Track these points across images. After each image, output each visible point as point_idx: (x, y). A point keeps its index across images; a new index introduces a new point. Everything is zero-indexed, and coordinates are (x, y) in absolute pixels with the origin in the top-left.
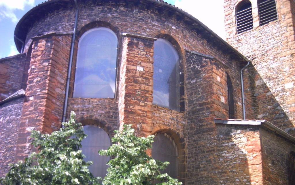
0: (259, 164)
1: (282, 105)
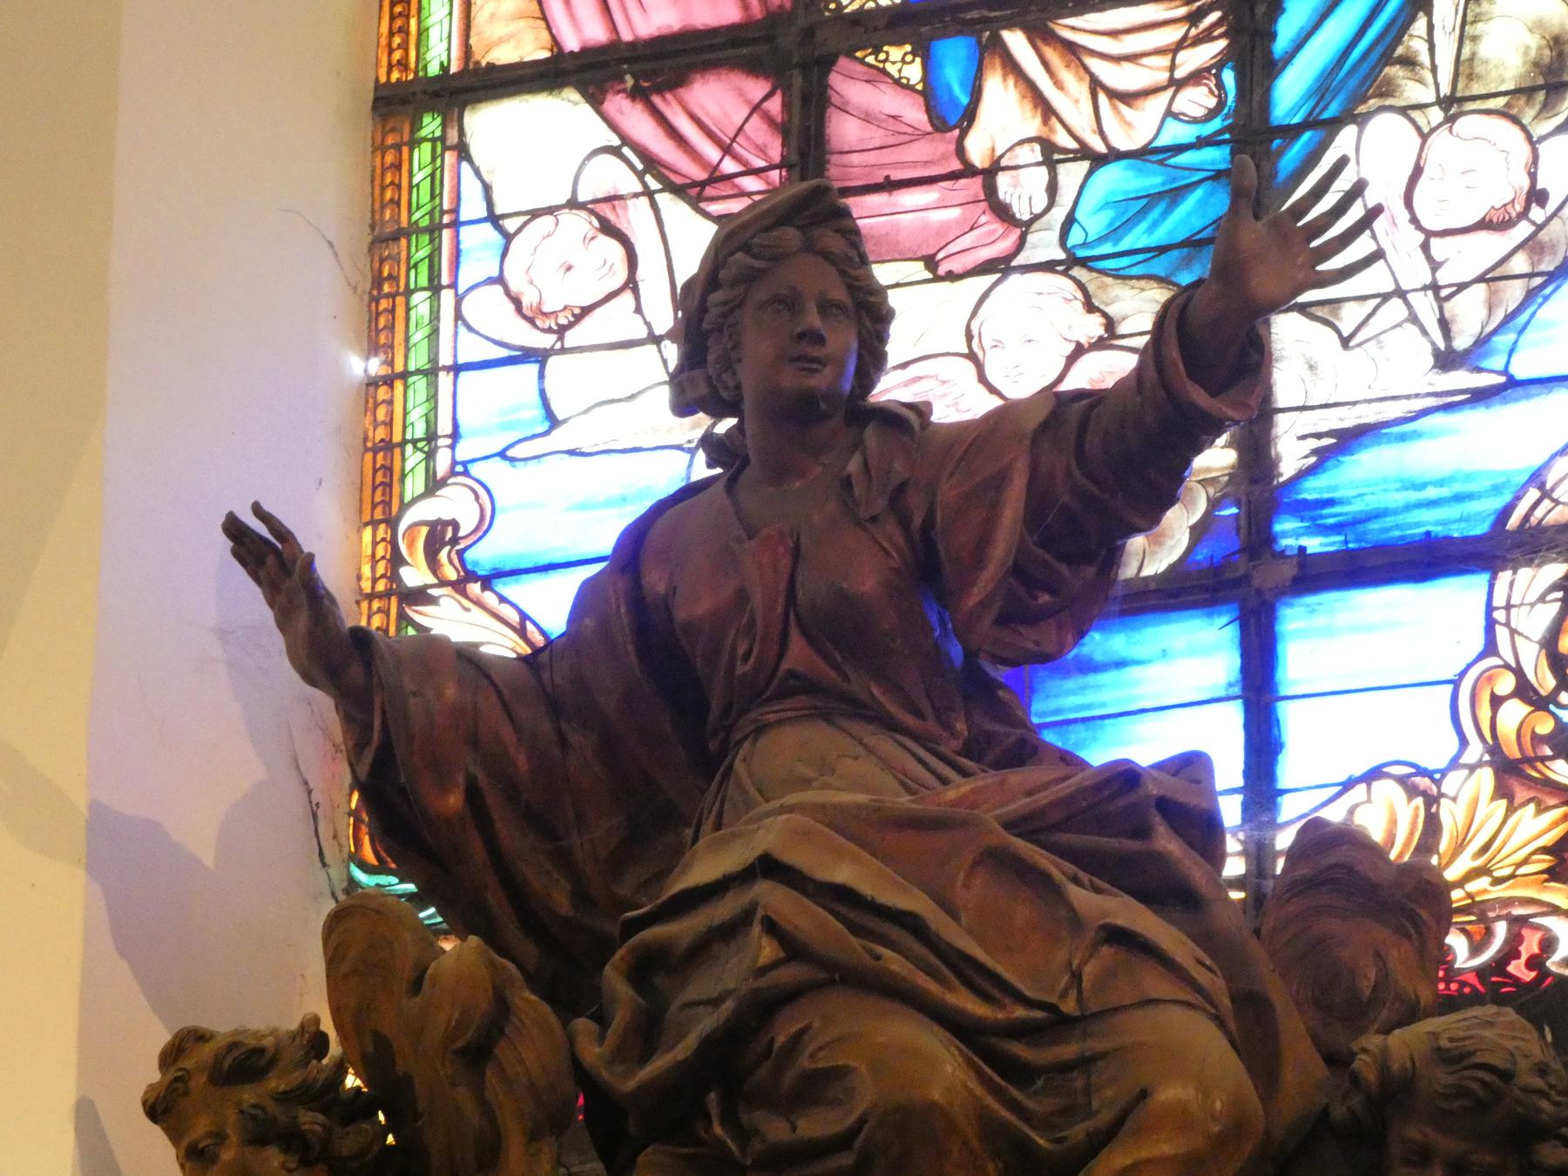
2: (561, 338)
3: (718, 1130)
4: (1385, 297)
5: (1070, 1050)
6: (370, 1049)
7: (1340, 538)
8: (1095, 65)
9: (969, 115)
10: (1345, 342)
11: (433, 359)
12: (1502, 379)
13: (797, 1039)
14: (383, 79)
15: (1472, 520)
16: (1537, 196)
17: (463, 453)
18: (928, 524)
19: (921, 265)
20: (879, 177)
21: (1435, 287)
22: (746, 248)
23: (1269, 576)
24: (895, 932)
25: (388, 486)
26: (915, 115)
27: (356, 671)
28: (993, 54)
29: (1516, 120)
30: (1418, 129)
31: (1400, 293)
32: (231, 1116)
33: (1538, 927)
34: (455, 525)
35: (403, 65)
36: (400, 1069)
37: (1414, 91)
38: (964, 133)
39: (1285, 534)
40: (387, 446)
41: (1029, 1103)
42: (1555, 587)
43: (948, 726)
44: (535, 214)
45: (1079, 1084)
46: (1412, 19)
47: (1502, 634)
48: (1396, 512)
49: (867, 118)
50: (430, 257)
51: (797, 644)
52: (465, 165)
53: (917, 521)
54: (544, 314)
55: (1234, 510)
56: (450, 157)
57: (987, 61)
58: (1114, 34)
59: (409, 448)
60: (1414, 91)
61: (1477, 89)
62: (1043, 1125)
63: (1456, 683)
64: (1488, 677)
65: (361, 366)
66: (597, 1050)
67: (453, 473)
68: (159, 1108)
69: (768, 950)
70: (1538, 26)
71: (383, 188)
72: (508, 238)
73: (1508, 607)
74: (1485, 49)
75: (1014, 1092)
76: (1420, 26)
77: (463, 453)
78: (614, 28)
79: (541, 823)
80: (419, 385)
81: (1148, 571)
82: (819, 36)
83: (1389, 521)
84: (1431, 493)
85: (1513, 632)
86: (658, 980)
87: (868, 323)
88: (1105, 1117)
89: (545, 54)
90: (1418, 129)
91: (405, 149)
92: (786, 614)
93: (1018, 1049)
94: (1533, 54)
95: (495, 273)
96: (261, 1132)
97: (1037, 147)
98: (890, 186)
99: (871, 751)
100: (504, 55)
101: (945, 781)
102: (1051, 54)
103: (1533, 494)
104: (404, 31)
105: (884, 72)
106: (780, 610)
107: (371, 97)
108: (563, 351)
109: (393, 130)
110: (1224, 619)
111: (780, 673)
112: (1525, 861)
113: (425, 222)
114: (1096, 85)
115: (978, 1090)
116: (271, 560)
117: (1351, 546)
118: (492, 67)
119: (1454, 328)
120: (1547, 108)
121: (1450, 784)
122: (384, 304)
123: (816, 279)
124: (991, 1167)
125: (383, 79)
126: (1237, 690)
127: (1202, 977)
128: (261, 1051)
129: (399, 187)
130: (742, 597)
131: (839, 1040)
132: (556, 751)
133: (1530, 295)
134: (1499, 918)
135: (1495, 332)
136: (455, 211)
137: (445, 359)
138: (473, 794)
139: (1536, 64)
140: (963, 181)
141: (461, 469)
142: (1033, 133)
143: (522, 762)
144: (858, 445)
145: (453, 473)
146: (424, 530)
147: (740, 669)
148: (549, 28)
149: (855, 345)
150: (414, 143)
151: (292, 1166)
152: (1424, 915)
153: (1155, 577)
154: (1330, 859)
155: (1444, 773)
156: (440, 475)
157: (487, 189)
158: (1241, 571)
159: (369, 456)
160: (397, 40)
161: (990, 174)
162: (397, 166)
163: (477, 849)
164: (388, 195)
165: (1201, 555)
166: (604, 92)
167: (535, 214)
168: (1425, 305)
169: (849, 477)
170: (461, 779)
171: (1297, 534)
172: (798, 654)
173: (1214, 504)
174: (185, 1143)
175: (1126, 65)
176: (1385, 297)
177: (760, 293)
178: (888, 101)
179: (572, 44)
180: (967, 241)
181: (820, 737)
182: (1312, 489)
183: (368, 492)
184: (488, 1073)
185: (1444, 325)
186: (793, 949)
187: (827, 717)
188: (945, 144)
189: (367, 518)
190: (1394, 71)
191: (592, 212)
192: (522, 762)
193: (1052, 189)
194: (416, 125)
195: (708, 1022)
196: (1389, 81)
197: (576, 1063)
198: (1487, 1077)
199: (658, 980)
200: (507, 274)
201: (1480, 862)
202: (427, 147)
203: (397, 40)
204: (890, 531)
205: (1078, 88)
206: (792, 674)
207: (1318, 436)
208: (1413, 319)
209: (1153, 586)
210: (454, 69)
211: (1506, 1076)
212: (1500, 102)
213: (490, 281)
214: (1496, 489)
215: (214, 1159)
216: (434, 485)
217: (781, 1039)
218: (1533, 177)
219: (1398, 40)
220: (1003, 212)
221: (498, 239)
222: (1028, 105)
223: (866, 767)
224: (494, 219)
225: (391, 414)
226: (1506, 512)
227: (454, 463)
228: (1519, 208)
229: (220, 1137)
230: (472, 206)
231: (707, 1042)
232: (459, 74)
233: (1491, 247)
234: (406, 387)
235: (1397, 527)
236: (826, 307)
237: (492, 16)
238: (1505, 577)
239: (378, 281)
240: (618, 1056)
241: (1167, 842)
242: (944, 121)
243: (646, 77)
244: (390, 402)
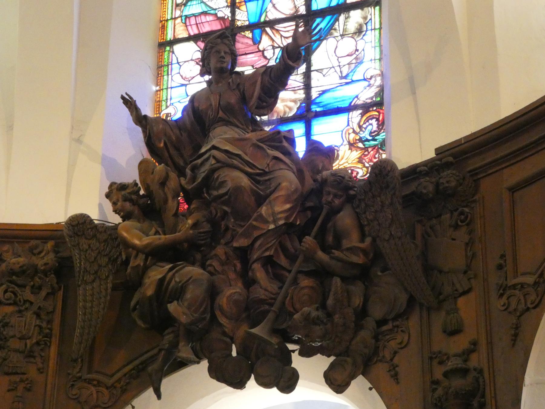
0: (187, 91)
1: (225, 65)
2: (189, 82)
3: (205, 195)
4: (331, 68)
5: (267, 178)
6: (146, 186)
7: (323, 108)
8: (281, 33)
9: (260, 42)
10: (324, 76)
11: (167, 87)
12: (351, 81)
13: (218, 177)
14: (160, 41)
15: (346, 104)
16: (357, 50)
17: (172, 102)
18: (244, 90)
19: (251, 67)
20: (244, 53)
21: (340, 66)
22: (211, 43)
23: (310, 115)
24: (235, 157)
25: (159, 108)
26: (250, 42)
27: (144, 122)
28: (264, 32)
29: (353, 38)
30: (337, 40)
31: (333, 67)
32: (120, 196)
33: (356, 171)
34: (171, 114)
35: (163, 39)
36: (151, 189)
37: (336, 34)
38: (259, 45)
39: (313, 108)
40: (159, 101)
41: (260, 187)
42: (360, 114)
43: (248, 128)
44: (185, 62)
45: (269, 183)
46: (336, 22)
47: (350, 122)
48: (332, 103)
49: (242, 43)
50: (167, 70)
51: (221, 112)
52: (173, 55)
53: (242, 90)
54: (187, 78)
55: (304, 105)
56: (171, 53)
57: (263, 33)
58: (285, 27)
59: (163, 101)
60: (336, 34)
61: (347, 33)
62: (261, 190)
63: (342, 131)
64: (348, 130)
65: (155, 88)
66: (184, 182)
67: (170, 105)
68: (108, 196)
69: (213, 162)
70: (357, 23)
71: (159, 59)
72: (181, 66)
73: (352, 118)
74: (348, 27)
75: (258, 185)
76: (337, 23)
77: (172, 102)
78: (199, 31)
79: (177, 149)
80: (165, 91)
81: (289, 116)
82: (234, 30)
83: (331, 105)
84: (338, 100)
85: (352, 122)
86: (196, 171)
87: (233, 57)
88: (273, 188)
89: (187, 36)
90: (337, 40)
91: (163, 53)
92: (219, 108)
93: (258, 178)
94: (356, 27)
95: (178, 72)
96: (125, 199)
97: (271, 47)
98: (246, 54)
99: (233, 130)
100: (180, 36)
101: (245, 134)
102: (274, 31)
103: (356, 99)
104: (164, 33)
105: (245, 35)
106: (217, 106)
107: (158, 44)
108: (190, 84)
109: (161, 49)
110: (303, 123)
111: (218, 117)
112: (354, 160)
113: (167, 64)
114: (281, 36)
115: (250, 184)
116: (129, 103)
117: (325, 109)
118: (178, 39)
119: (343, 73)
120: (359, 36)
121: (341, 148)
122: (159, 78)
123: (223, 48)
124: (253, 198)
125: (160, 41)
126: (304, 134)
127: (291, 165)
128: (125, 185)
129: (162, 59)
130: (211, 105)
131: (225, 176)
132: (180, 137)
133: (356, 67)
134: (349, 170)
135: (350, 73)
136: (172, 62)
137: (169, 86)
138: (165, 144)
139: (357, 29)
140: (258, 53)
141: (172, 104)
142: (271, 44)
143: (174, 138)
144: (231, 77)
145: (170, 105)
146: (165, 115)
147: (211, 117)
148: (188, 31)
149: (231, 60)
150: (165, 51)
151: (131, 205)
152: (331, 154)
153: (291, 117)
154: (314, 146)
155: (340, 146)
156: (168, 106)
157: (177, 58)
158: (306, 114)
159: (156, 103)
160: (162, 35)
161: (263, 51)
162: (162, 55)
163: (166, 154)
164: (160, 60)
165: (299, 112)
166: (197, 41)
167: (185, 62)
168: (338, 69)
169: (229, 82)
170: (163, 141)
171: (315, 108)
172: (221, 114)
173: (301, 104)
174: (113, 201)
175: (287, 33)
176: (331, 68)
177: (214, 50)
178: (246, 41)
179: (192, 34)
180: (259, 62)
181: (224, 128)
182: (318, 101)
183: (156, 109)
184: (165, 187)
185: (341, 72)
186: (218, 161)
187: (226, 125)
188: (256, 47)
189: (155, 113)
190: (333, 31)
191: (195, 61)
192: (174, 138)
193: (274, 53)
194: (165, 48)
195: (203, 175)
196: (332, 33)
197: (181, 185)
198: (340, 178)
199: (196, 171)
200: (180, 72)
201: (346, 161)
202: (167, 52)
203: (162, 35)
204: (237, 92)
205: (278, 36)
206: (220, 117)
207: (319, 91)
208: (336, 71)
209: (290, 118)
210: (172, 39)
211: (343, 178)
212: (351, 35)
213: (178, 73)
214: (350, 99)
215: (117, 204)
216: (167, 107)
217: (216, 177)
218: (356, 47)
219: (333, 26)
220: (265, 57)
221: (179, 66)
222: (270, 40)
223: (232, 132)
224: (178, 63)
225: (160, 96)
226: (351, 102)
227: (171, 103)
228: (354, 52)
229: (118, 200)
230: (175, 61)
231: (203, 178)
232: (173, 40)
233: (349, 59)
234: (163, 91)
235: (332, 106)
236: (225, 53)
237: (179, 30)
238: (351, 113)
239: (158, 74)
240: (187, 183)
241: (285, 144)
242: (255, 43)
243: (205, 39)
244: (160, 94)
